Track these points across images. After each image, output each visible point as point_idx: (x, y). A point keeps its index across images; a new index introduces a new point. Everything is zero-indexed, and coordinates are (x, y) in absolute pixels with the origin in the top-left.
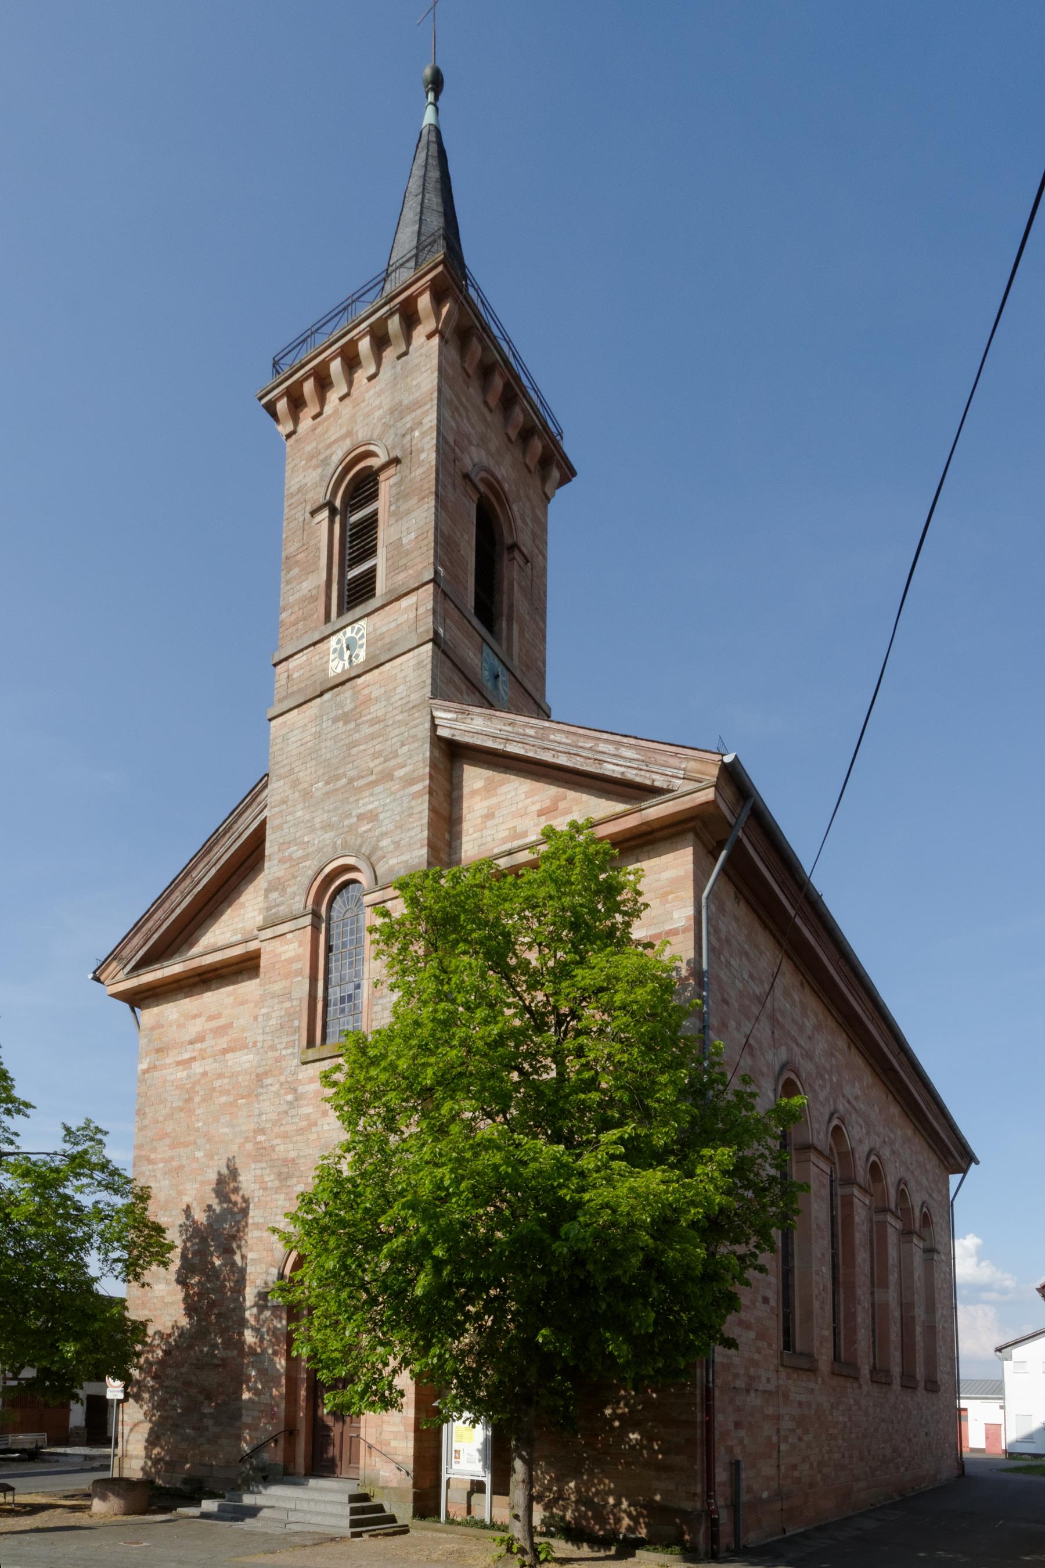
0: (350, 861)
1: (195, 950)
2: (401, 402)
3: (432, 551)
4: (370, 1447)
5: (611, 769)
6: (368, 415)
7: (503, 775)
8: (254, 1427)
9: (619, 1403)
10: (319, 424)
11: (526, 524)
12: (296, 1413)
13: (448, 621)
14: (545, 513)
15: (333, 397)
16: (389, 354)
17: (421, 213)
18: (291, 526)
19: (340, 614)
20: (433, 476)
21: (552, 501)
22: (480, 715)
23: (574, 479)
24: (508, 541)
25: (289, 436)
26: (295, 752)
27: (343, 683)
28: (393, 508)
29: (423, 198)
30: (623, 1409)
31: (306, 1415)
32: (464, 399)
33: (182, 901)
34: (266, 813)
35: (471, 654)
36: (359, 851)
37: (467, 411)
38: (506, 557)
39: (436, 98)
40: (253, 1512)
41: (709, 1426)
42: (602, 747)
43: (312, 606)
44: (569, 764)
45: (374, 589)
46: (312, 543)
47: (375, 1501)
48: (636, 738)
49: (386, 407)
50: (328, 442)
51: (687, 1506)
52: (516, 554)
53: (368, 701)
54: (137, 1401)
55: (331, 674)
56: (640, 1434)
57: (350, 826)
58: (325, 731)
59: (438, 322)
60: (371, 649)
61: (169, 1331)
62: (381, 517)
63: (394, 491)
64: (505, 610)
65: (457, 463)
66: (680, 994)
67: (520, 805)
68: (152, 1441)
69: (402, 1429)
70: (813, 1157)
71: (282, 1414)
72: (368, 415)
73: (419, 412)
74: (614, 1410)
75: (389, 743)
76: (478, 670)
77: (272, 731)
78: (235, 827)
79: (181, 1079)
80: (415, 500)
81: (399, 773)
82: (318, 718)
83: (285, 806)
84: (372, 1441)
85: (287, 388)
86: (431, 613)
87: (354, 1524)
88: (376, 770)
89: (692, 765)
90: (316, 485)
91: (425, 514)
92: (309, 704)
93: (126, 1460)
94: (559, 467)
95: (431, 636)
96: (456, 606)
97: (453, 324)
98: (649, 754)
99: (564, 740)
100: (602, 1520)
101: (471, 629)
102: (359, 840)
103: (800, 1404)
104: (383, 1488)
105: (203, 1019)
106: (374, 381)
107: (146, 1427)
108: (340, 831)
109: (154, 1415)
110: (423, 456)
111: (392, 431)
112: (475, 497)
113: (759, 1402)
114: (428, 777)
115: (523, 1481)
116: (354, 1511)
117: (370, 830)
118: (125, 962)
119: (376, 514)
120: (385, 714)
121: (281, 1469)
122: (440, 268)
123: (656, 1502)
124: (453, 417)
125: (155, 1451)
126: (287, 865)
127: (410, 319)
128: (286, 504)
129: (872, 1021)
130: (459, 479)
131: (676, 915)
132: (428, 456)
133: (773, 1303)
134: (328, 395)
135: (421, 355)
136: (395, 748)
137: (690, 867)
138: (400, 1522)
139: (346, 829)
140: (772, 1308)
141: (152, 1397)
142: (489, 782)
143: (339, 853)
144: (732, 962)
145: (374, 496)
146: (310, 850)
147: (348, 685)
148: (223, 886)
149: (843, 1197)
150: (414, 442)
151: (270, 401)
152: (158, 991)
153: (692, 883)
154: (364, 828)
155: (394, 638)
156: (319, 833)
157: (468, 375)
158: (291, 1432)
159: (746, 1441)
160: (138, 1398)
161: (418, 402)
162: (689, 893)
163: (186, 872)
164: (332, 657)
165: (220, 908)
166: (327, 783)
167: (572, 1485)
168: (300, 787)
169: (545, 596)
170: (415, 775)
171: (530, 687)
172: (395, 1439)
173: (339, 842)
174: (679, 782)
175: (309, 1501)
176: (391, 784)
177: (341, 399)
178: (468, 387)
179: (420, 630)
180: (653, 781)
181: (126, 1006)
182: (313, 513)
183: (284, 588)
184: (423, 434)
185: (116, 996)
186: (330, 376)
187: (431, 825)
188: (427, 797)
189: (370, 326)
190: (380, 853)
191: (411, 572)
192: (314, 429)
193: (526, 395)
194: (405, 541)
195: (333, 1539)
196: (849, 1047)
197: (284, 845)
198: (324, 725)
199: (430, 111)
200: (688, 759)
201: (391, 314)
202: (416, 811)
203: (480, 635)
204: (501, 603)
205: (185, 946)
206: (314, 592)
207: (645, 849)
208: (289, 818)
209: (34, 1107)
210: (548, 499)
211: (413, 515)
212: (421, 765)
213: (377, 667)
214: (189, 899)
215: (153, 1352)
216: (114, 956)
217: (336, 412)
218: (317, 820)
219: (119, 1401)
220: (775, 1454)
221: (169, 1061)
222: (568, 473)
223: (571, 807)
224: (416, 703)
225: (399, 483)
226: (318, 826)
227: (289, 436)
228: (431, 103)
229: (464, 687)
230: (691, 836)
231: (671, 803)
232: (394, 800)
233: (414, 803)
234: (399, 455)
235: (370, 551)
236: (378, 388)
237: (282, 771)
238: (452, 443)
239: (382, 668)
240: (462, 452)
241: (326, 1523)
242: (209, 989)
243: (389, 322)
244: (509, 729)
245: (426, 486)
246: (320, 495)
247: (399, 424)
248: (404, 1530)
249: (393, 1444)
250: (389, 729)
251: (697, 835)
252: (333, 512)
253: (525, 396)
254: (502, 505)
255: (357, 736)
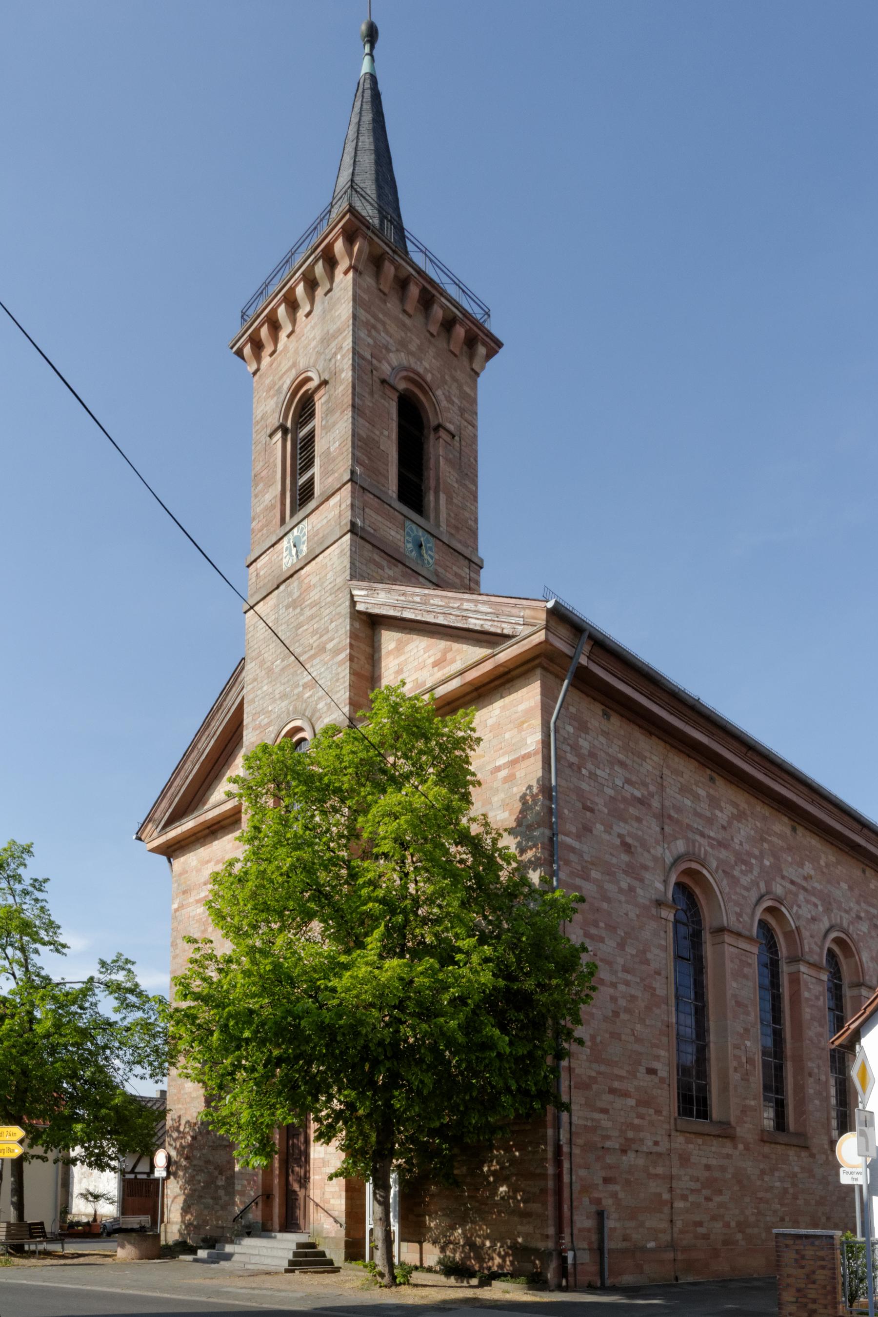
0: (298, 723)
1: (206, 807)
2: (328, 332)
3: (350, 455)
4: (317, 1205)
5: (474, 623)
6: (306, 347)
7: (409, 636)
8: (242, 1194)
9: (492, 1161)
10: (275, 360)
11: (452, 403)
12: (272, 1180)
13: (367, 510)
14: (474, 387)
15: (283, 335)
16: (320, 292)
17: (355, 156)
18: (258, 448)
19: (292, 515)
20: (350, 391)
21: (482, 375)
22: (382, 589)
23: (501, 351)
24: (433, 422)
25: (255, 373)
26: (262, 637)
27: (291, 576)
28: (324, 423)
29: (357, 142)
30: (495, 1167)
31: (279, 1182)
32: (381, 316)
33: (193, 769)
34: (245, 691)
35: (393, 533)
36: (304, 715)
37: (384, 324)
38: (432, 436)
39: (372, 48)
40: (228, 1257)
41: (559, 1176)
42: (466, 606)
43: (272, 514)
44: (445, 623)
45: (313, 494)
46: (272, 460)
47: (320, 1248)
48: (487, 595)
49: (318, 338)
50: (281, 373)
51: (541, 1246)
52: (442, 433)
53: (309, 587)
54: (175, 1178)
55: (284, 568)
56: (508, 1186)
57: (298, 694)
58: (281, 617)
59: (351, 260)
60: (310, 544)
61: (195, 1121)
62: (317, 433)
63: (325, 408)
64: (432, 483)
65: (374, 372)
66: (532, 809)
67: (420, 660)
68: (186, 1210)
69: (337, 1189)
70: (728, 938)
71: (260, 1181)
72: (306, 347)
73: (340, 338)
74: (489, 1167)
75: (323, 621)
76: (401, 544)
77: (247, 621)
78: (225, 704)
79: (200, 914)
80: (338, 414)
81: (330, 646)
82: (277, 606)
83: (255, 683)
84: (317, 1201)
85: (249, 336)
86: (349, 508)
87: (291, 1263)
88: (314, 645)
89: (528, 613)
90: (273, 412)
91: (345, 424)
92: (271, 596)
93: (169, 1226)
94: (485, 344)
95: (349, 528)
96: (375, 495)
97: (365, 256)
98: (498, 607)
99: (440, 603)
100: (480, 1259)
101: (392, 510)
102: (304, 705)
103: (708, 1167)
104: (325, 1238)
105: (213, 863)
106: (310, 317)
107: (181, 1199)
108: (292, 699)
109: (186, 1189)
110: (343, 375)
111: (322, 357)
112: (395, 396)
113: (641, 1162)
114: (348, 647)
115: (381, 1219)
116: (295, 1254)
117: (311, 696)
118: (157, 822)
119: (314, 431)
120: (320, 598)
121: (260, 1225)
122: (348, 216)
123: (520, 1244)
124: (370, 335)
125: (187, 1218)
126: (258, 732)
127: (331, 262)
128: (254, 431)
129: (812, 802)
130: (377, 386)
131: (529, 742)
132: (347, 375)
133: (663, 1073)
134: (280, 334)
135: (341, 290)
136: (326, 625)
137: (539, 697)
138: (336, 1265)
139: (295, 697)
140: (662, 1080)
141: (184, 1174)
142: (399, 642)
143: (292, 717)
144: (599, 772)
145: (312, 415)
146: (272, 717)
147: (295, 576)
148: (224, 750)
149: (790, 974)
150: (338, 364)
151: (238, 348)
152: (183, 843)
153: (540, 712)
154: (307, 695)
155: (325, 533)
156: (278, 702)
157: (385, 294)
158: (267, 1196)
159: (621, 1195)
160: (175, 1175)
161: (339, 330)
162: (537, 721)
163: (193, 745)
164: (285, 554)
165: (223, 770)
166: (283, 661)
167: (460, 1231)
168: (265, 666)
169: (476, 461)
170: (340, 646)
171: (459, 547)
172: (333, 1198)
173: (291, 708)
174: (521, 628)
175: (272, 1248)
176: (324, 655)
177: (289, 336)
178: (385, 302)
179: (342, 523)
180: (503, 629)
181: (164, 859)
182: (271, 435)
183: (254, 501)
184: (343, 357)
185: (154, 850)
186: (278, 320)
187: (352, 687)
188: (348, 664)
189: (303, 274)
190: (318, 714)
191: (336, 475)
192: (271, 365)
193: (443, 292)
194: (332, 449)
195: (268, 1273)
196: (794, 829)
197: (256, 715)
198: (281, 612)
199: (367, 59)
200: (524, 608)
201: (316, 261)
202: (341, 676)
203: (402, 514)
204: (429, 478)
205: (201, 805)
206: (273, 501)
207: (507, 686)
208: (259, 692)
209: (69, 948)
210: (477, 374)
211: (337, 427)
212: (343, 637)
213: (314, 559)
214: (197, 767)
215: (185, 1138)
216: (149, 819)
217: (286, 347)
218: (277, 692)
219: (164, 1180)
220: (666, 1210)
221: (191, 900)
222: (494, 345)
223: (455, 657)
224: (340, 585)
225: (328, 401)
226: (277, 696)
227: (255, 373)
228: (367, 54)
229: (385, 563)
230: (539, 672)
231: (515, 647)
232: (327, 669)
233: (340, 670)
234: (327, 378)
235: (309, 463)
236: (313, 322)
237: (254, 654)
238: (369, 357)
239: (317, 559)
240: (380, 362)
241: (273, 1263)
242: (216, 839)
243: (316, 267)
244: (402, 598)
245: (346, 400)
246: (274, 420)
247: (327, 351)
248: (337, 1270)
249: (332, 1201)
250: (322, 610)
251: (545, 669)
252: (285, 431)
253: (441, 294)
254: (425, 393)
255: (302, 618)
